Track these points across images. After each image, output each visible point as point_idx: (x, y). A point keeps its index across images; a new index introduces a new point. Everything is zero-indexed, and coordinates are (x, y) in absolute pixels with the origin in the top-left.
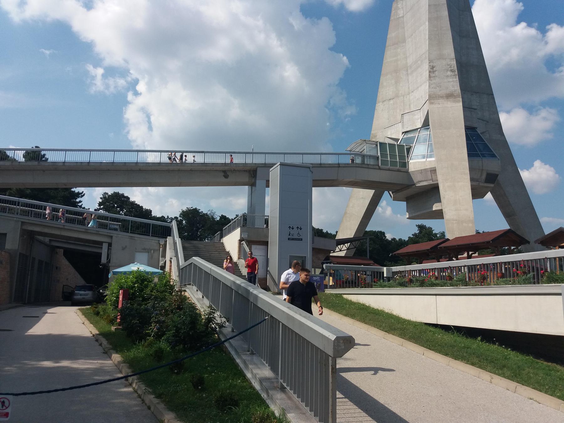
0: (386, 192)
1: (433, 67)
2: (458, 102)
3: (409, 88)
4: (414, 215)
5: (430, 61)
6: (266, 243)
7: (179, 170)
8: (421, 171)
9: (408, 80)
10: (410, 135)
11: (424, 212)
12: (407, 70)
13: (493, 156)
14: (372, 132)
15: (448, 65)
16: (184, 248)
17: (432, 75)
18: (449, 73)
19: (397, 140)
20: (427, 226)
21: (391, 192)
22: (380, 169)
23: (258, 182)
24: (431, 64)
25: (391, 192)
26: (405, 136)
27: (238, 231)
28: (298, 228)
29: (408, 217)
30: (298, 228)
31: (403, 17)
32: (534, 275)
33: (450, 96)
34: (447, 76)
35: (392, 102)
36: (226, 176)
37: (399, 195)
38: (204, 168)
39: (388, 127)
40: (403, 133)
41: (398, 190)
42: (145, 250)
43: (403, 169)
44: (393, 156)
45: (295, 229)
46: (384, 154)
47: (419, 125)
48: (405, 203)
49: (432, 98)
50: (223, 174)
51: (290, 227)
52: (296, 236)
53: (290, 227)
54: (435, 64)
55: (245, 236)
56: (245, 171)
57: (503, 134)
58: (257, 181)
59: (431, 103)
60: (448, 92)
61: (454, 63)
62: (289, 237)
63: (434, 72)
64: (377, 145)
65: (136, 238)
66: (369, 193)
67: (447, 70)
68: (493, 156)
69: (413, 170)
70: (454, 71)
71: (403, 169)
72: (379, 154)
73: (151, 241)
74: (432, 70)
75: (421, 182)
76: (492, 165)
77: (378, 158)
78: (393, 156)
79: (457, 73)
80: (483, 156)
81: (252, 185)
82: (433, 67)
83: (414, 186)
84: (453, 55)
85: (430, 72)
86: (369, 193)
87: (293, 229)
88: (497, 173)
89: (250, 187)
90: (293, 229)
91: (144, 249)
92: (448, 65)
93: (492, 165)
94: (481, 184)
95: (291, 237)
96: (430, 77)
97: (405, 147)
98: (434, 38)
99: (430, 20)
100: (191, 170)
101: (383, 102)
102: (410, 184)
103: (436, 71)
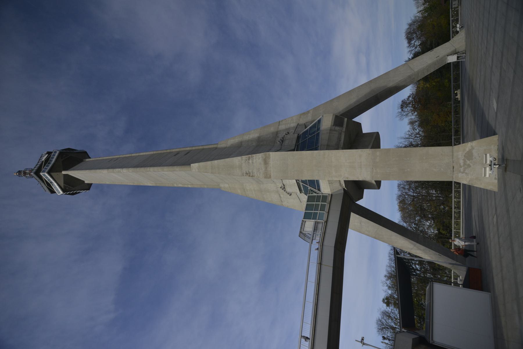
1: (247, 173)
2: (269, 155)
13: (319, 121)
18: (250, 161)
22: (326, 222)
24: (245, 174)
33: (266, 162)
34: (252, 163)
35: (282, 196)
48: (365, 190)
60: (263, 163)
61: (244, 157)
63: (250, 173)
66: (354, 219)
67: (249, 163)
68: (319, 121)
69: (329, 190)
70: (249, 157)
75: (340, 184)
79: (250, 156)
80: (318, 129)
86: (354, 219)
94: (344, 129)
101: (282, 201)
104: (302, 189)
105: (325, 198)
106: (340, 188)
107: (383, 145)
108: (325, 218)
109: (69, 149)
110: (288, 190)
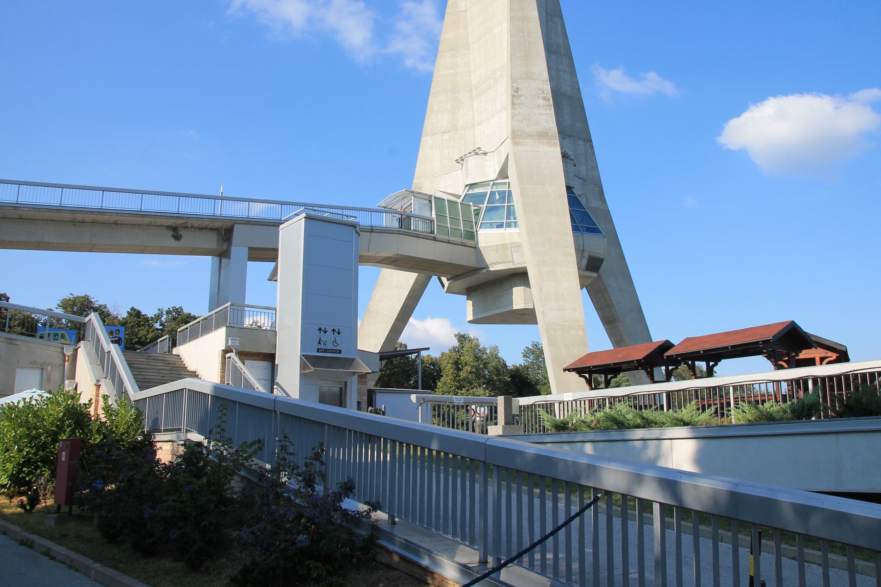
0: (434, 279)
1: (517, 90)
3: (473, 118)
4: (479, 316)
5: (513, 80)
6: (270, 358)
7: (93, 222)
8: (497, 248)
9: (472, 106)
10: (476, 191)
11: (498, 311)
12: (471, 91)
14: (415, 181)
15: (539, 89)
16: (131, 365)
17: (517, 101)
18: (541, 102)
19: (459, 197)
20: (472, 336)
21: (444, 279)
22: (435, 239)
23: (234, 250)
24: (515, 85)
25: (444, 279)
26: (471, 192)
27: (222, 331)
28: (334, 330)
29: (470, 317)
30: (334, 330)
31: (466, 10)
32: (717, 409)
33: (542, 136)
34: (539, 106)
35: (446, 137)
36: (177, 238)
37: (462, 284)
38: (140, 220)
39: (441, 172)
40: (467, 186)
41: (458, 276)
42: (34, 364)
43: (470, 243)
44: (454, 219)
45: (330, 332)
46: (440, 215)
47: (493, 176)
49: (517, 136)
50: (171, 233)
51: (320, 329)
52: (330, 346)
53: (320, 329)
54: (520, 86)
55: (235, 343)
56: (212, 229)
57: (604, 201)
58: (233, 248)
59: (515, 144)
61: (547, 87)
62: (320, 346)
63: (519, 97)
64: (430, 201)
65: (18, 343)
67: (539, 97)
71: (470, 243)
72: (434, 216)
73: (44, 349)
74: (516, 94)
75: (495, 264)
76: (597, 245)
77: (432, 221)
78: (454, 219)
81: (223, 254)
82: (517, 90)
83: (485, 270)
84: (545, 75)
85: (513, 96)
86: (409, 278)
87: (325, 332)
88: (601, 256)
89: (217, 259)
90: (325, 332)
91: (34, 362)
92: (539, 89)
93: (597, 245)
95: (322, 346)
96: (513, 104)
97: (473, 208)
98: (518, 49)
99: (512, 19)
100: (116, 223)
102: (480, 268)
103: (521, 96)
104: (476, 191)
105: (472, 236)
106: (488, 262)
107: (752, 575)
108: (439, 237)
109: (687, 339)
110: (472, 161)
